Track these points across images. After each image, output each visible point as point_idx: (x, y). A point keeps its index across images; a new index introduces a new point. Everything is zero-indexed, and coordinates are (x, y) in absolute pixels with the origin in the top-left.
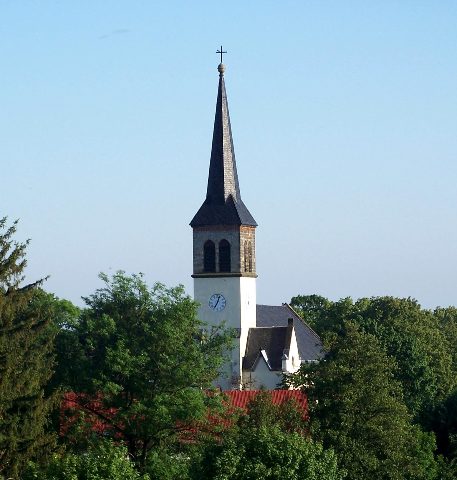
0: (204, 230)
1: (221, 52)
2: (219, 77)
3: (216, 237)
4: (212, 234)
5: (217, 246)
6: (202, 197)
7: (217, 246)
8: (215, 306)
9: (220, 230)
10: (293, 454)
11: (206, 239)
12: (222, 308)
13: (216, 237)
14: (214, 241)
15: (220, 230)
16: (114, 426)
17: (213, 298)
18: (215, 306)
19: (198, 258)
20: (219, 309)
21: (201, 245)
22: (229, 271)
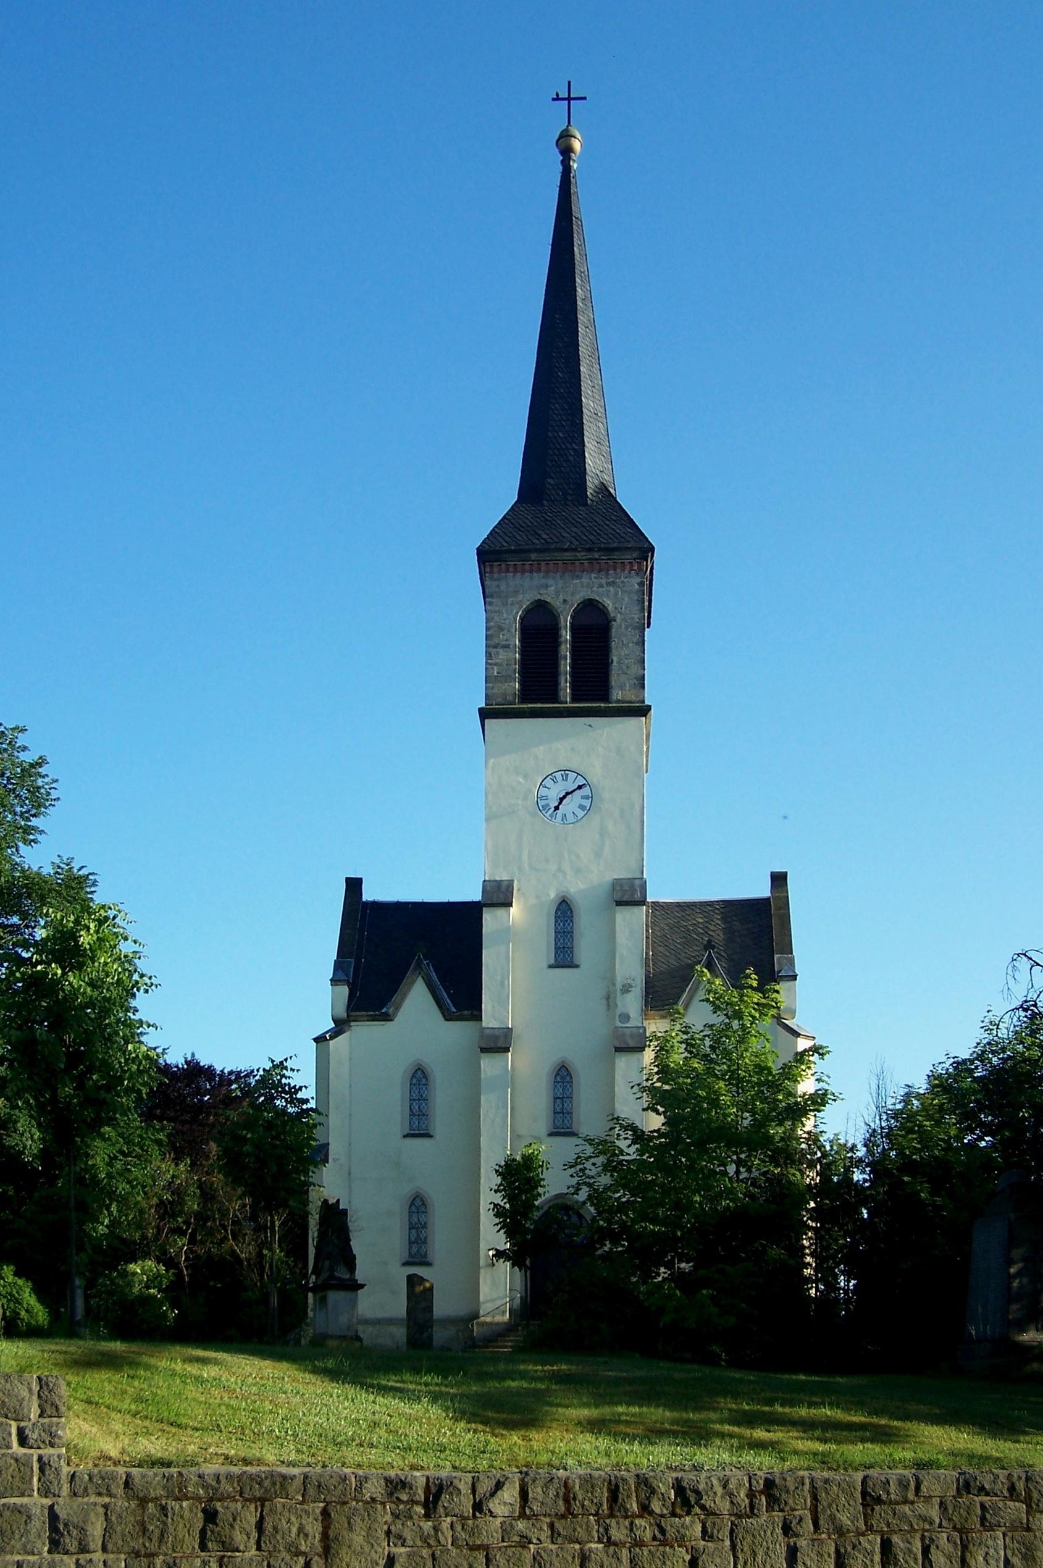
0: (523, 572)
1: (569, 99)
2: (560, 168)
3: (565, 594)
4: (550, 582)
5: (566, 621)
6: (511, 497)
7: (566, 621)
8: (557, 808)
9: (273, 1061)
10: (73, 889)
11: (527, 599)
12: (580, 813)
13: (565, 594)
14: (556, 603)
15: (273, 1061)
16: (704, 1540)
17: (548, 782)
18: (557, 808)
19: (503, 655)
20: (571, 818)
21: (513, 618)
22: (606, 698)
